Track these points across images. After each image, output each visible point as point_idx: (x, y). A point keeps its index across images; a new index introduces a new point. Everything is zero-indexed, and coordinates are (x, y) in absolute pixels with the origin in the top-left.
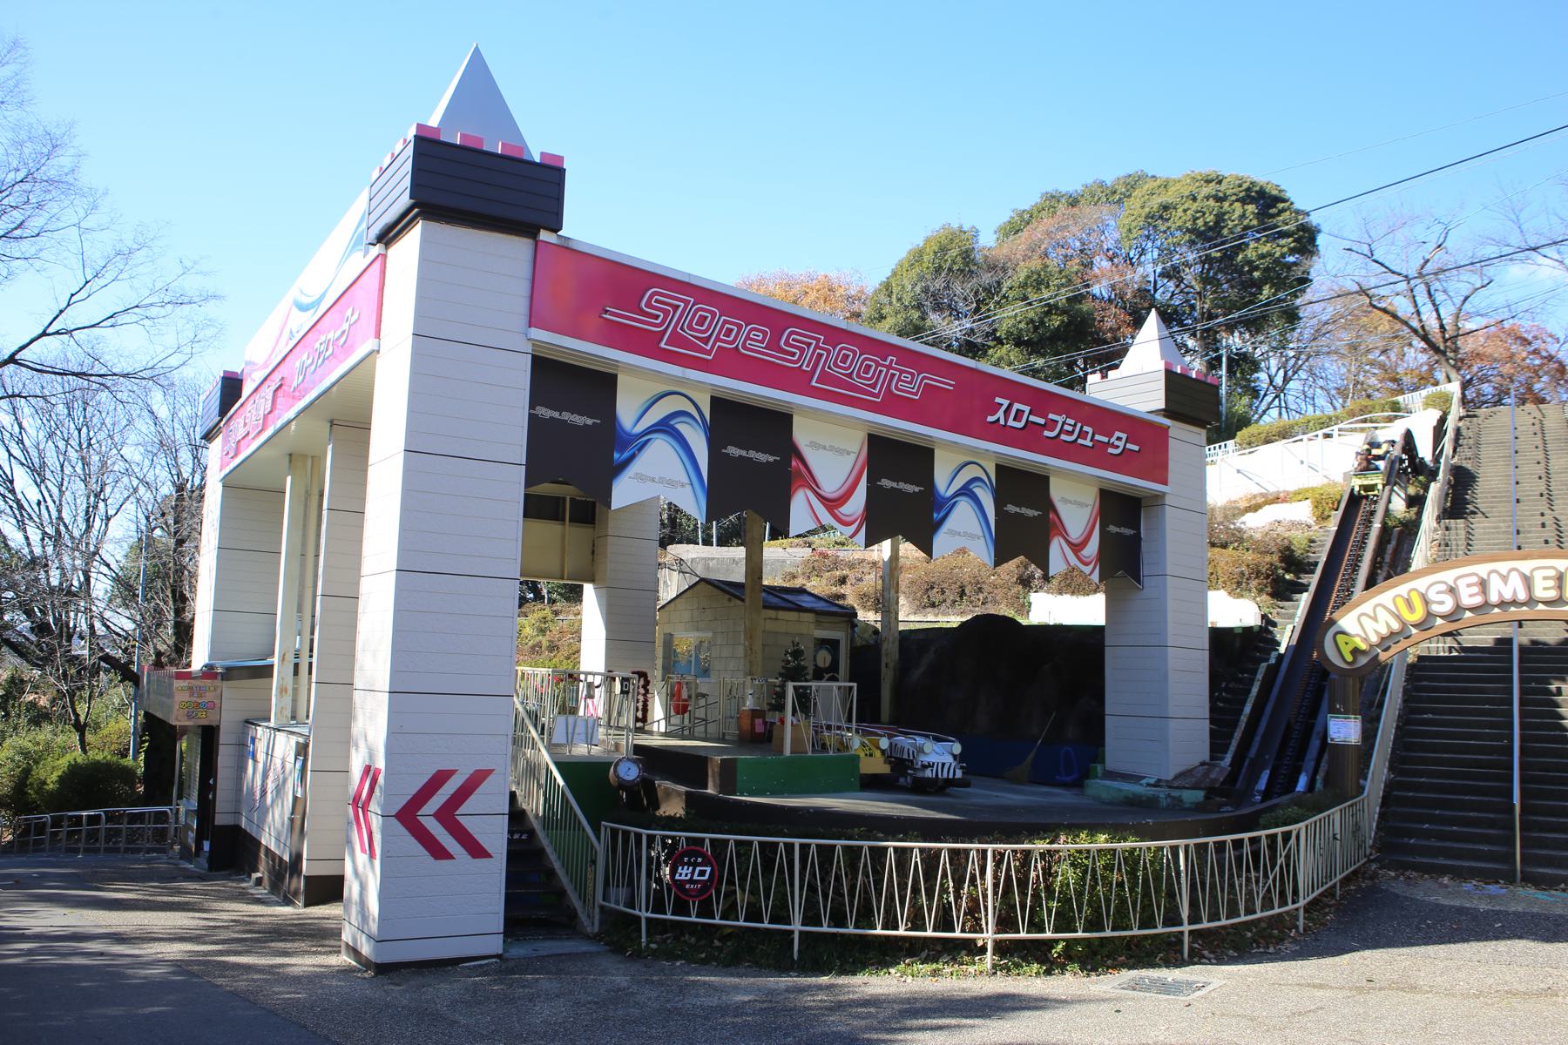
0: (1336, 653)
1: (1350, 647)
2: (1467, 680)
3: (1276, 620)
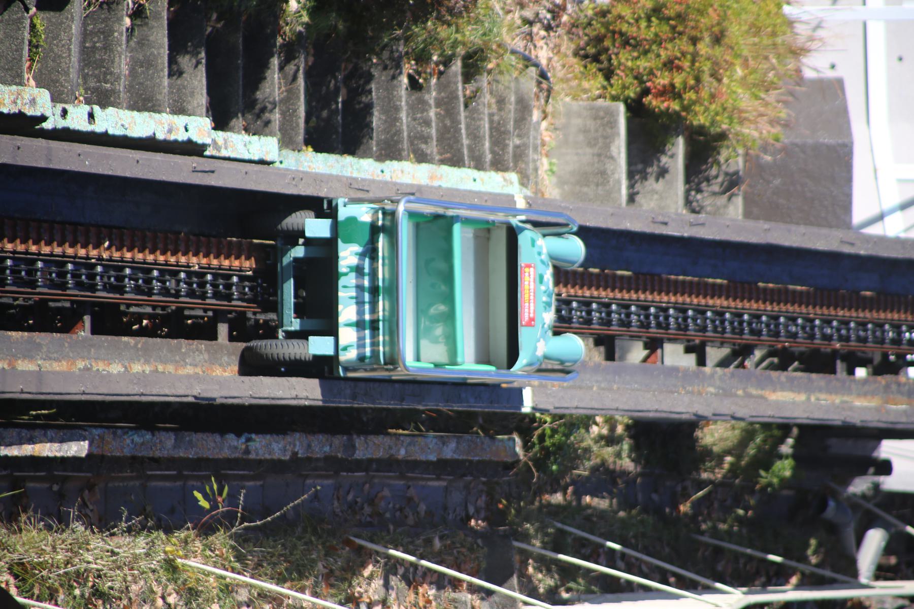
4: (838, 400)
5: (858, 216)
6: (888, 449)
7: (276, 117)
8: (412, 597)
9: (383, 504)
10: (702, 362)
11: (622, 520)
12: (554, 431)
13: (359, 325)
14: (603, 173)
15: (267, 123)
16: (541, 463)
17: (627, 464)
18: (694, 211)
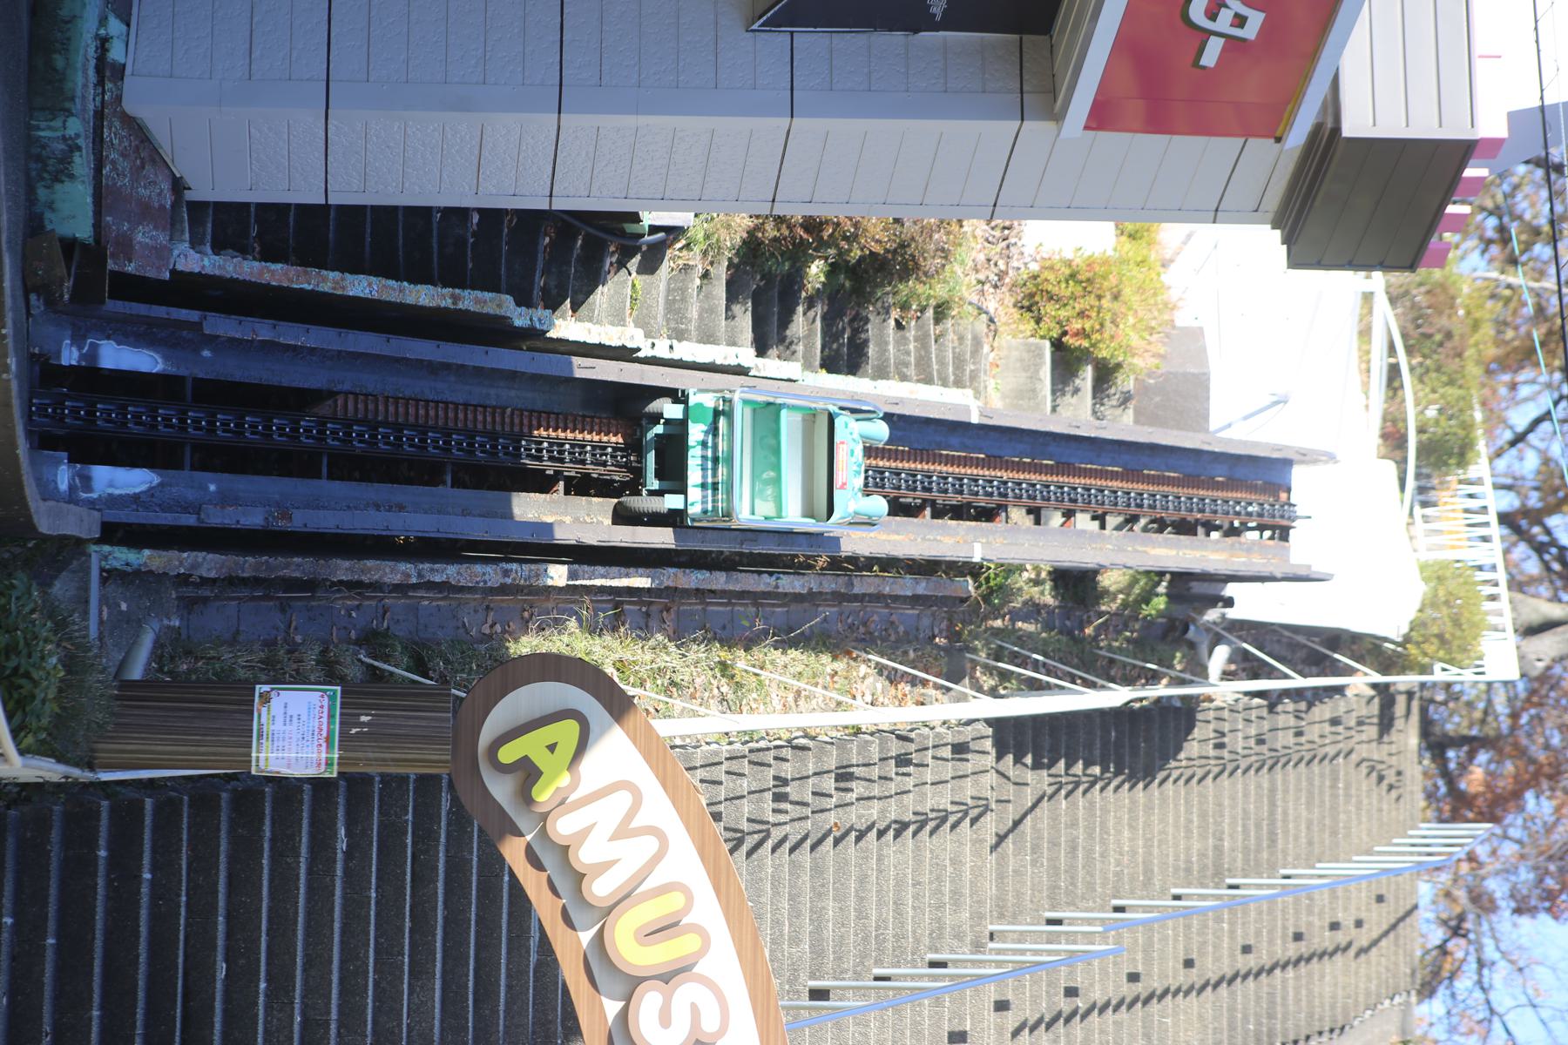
0: (524, 716)
1: (540, 759)
2: (455, 923)
3: (666, 266)
4: (1198, 554)
5: (1213, 426)
6: (1231, 590)
7: (800, 348)
8: (893, 691)
9: (873, 626)
10: (1103, 527)
11: (1044, 639)
12: (996, 575)
13: (704, 486)
14: (1034, 391)
15: (794, 352)
16: (987, 598)
17: (1049, 599)
18: (1098, 419)
